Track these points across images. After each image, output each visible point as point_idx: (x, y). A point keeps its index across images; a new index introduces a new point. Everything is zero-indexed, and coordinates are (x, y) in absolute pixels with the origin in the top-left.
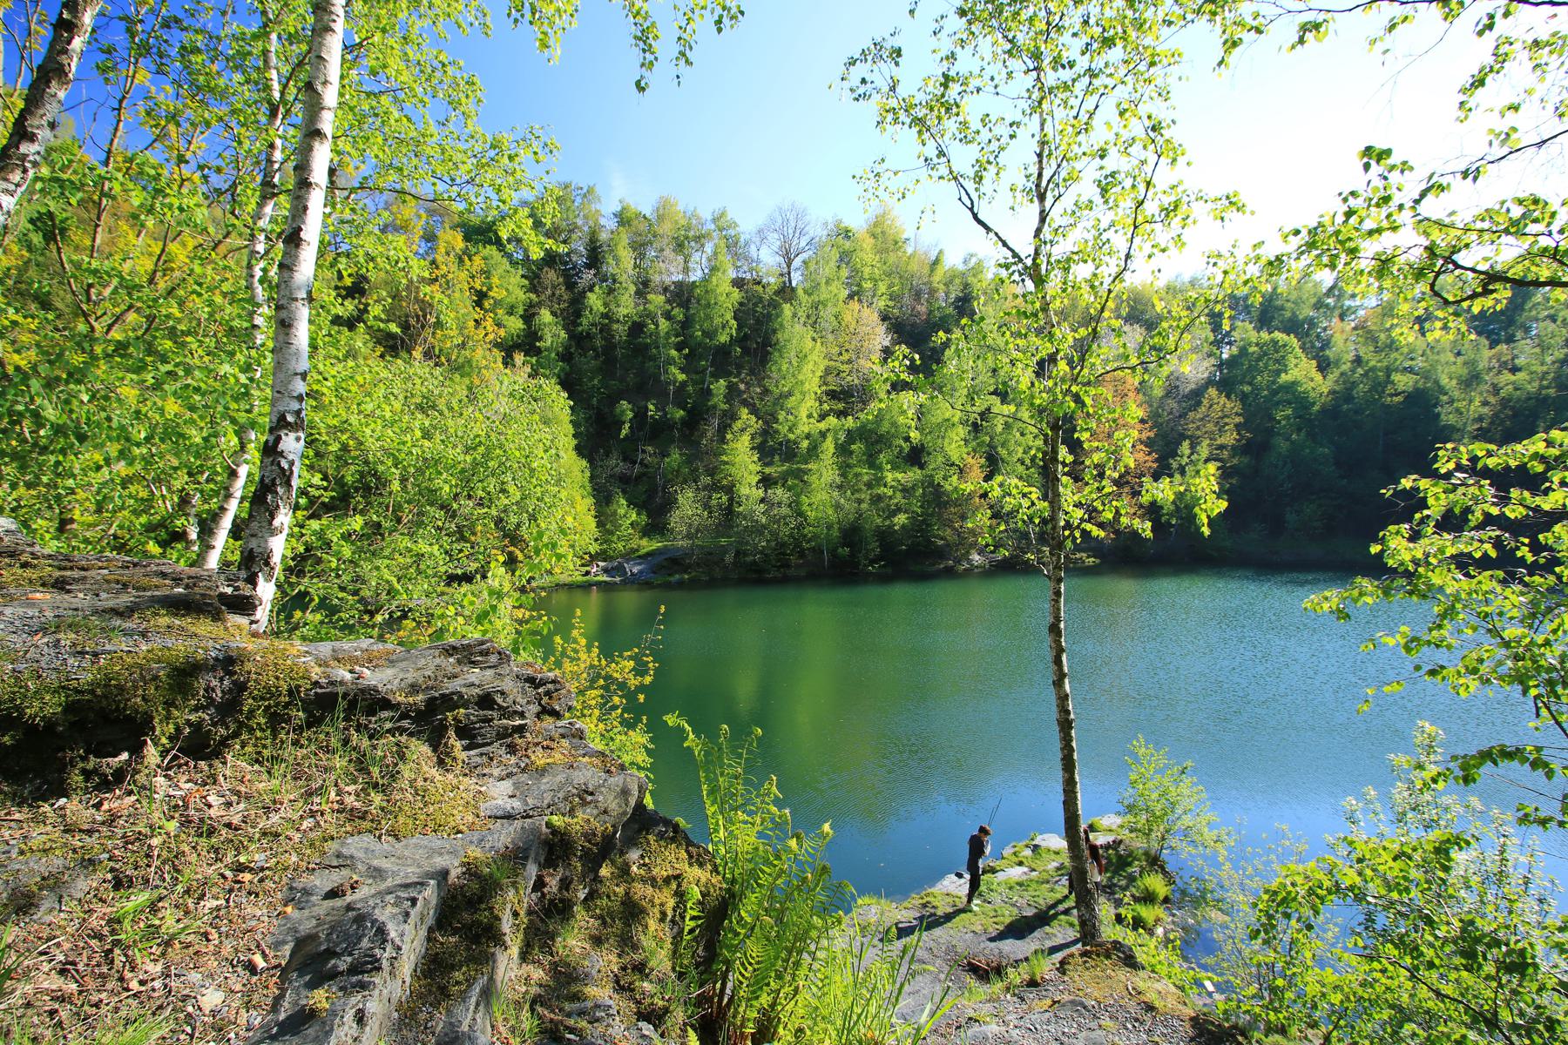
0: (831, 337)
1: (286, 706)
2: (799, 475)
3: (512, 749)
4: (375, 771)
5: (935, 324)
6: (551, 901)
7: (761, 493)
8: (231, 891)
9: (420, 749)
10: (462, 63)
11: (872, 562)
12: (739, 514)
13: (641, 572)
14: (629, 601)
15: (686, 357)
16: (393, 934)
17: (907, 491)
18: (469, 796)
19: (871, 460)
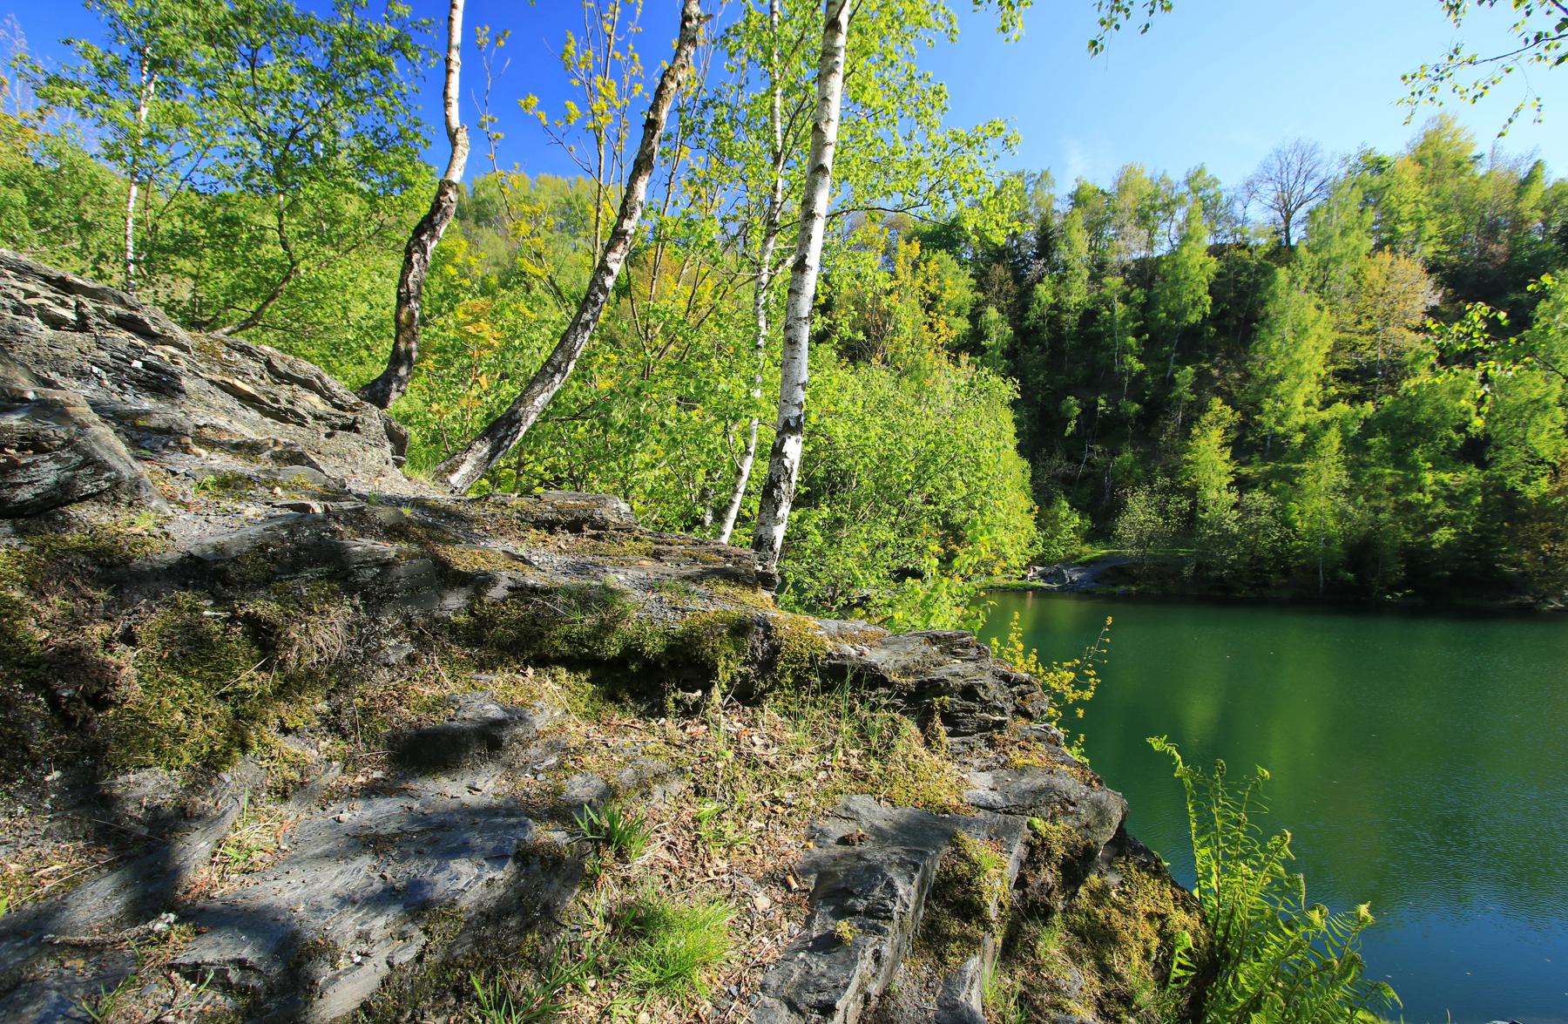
0: (1345, 303)
1: (807, 670)
2: (1288, 476)
3: (991, 743)
4: (874, 740)
5: (1522, 268)
6: (1033, 903)
7: (1234, 497)
8: (769, 817)
9: (910, 727)
10: (931, 75)
11: (1391, 590)
12: (1204, 521)
13: (1080, 580)
14: (1066, 611)
15: (1146, 343)
16: (901, 892)
17: (1451, 498)
18: (953, 781)
19: (1399, 457)
